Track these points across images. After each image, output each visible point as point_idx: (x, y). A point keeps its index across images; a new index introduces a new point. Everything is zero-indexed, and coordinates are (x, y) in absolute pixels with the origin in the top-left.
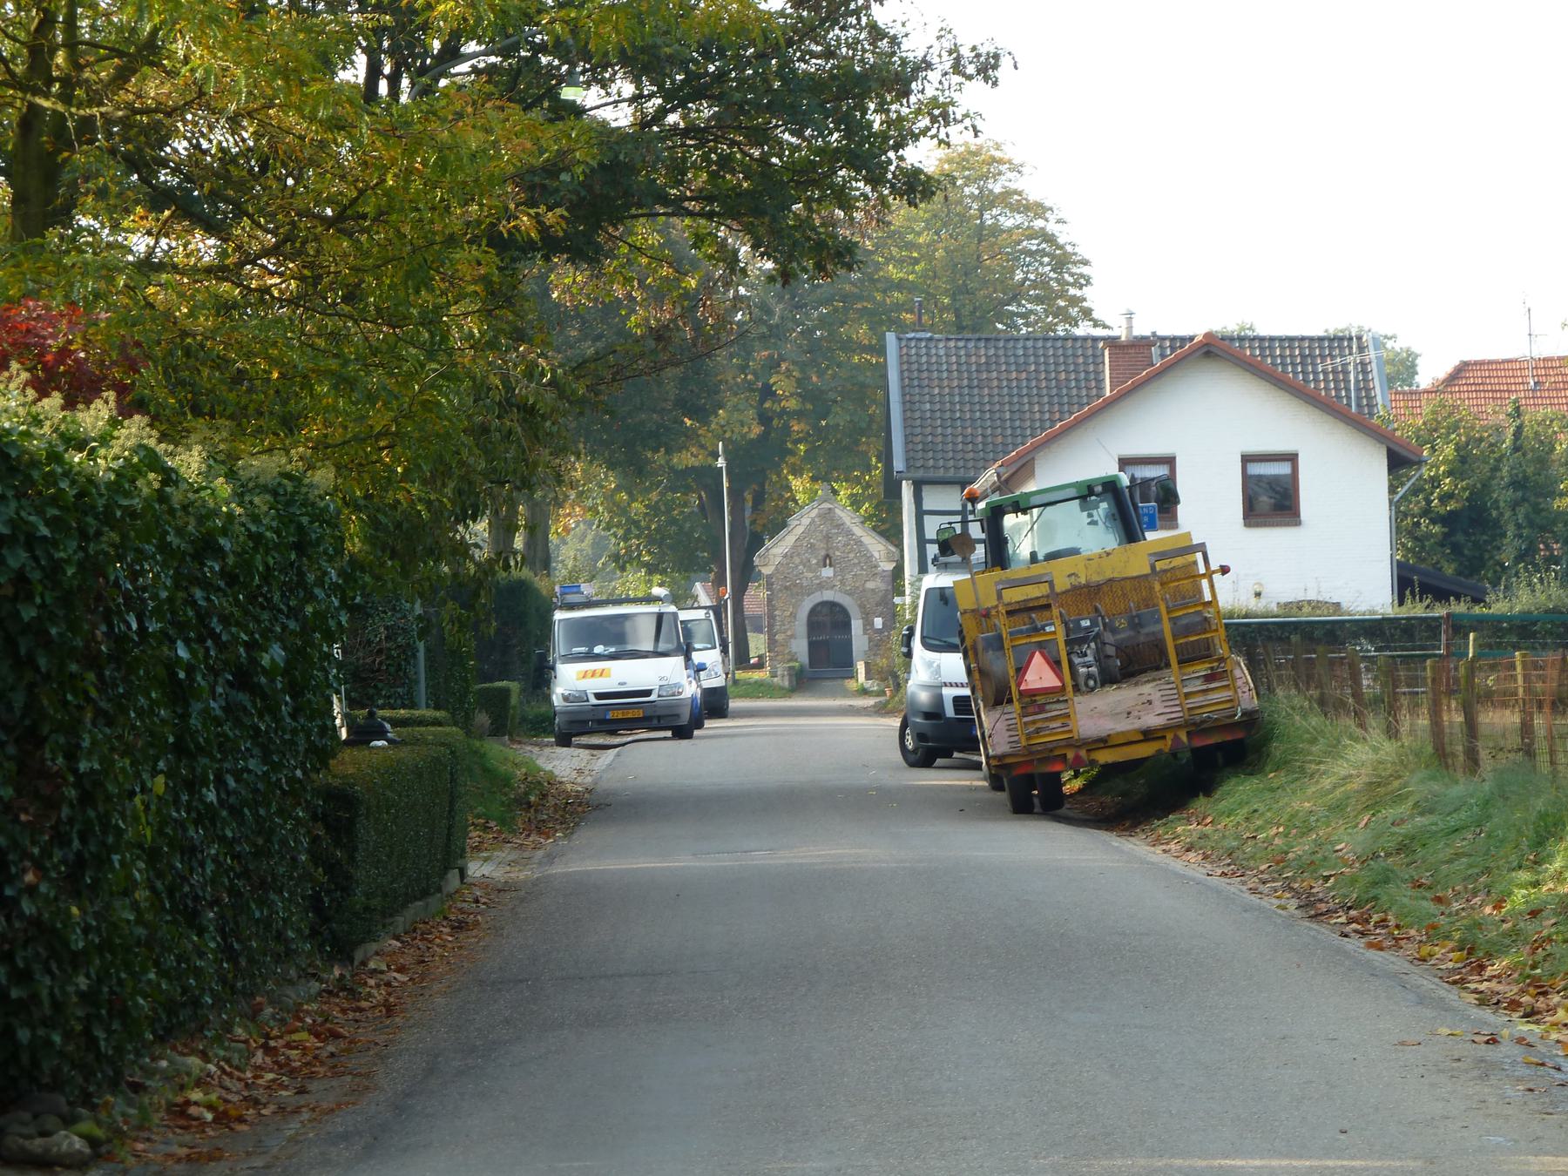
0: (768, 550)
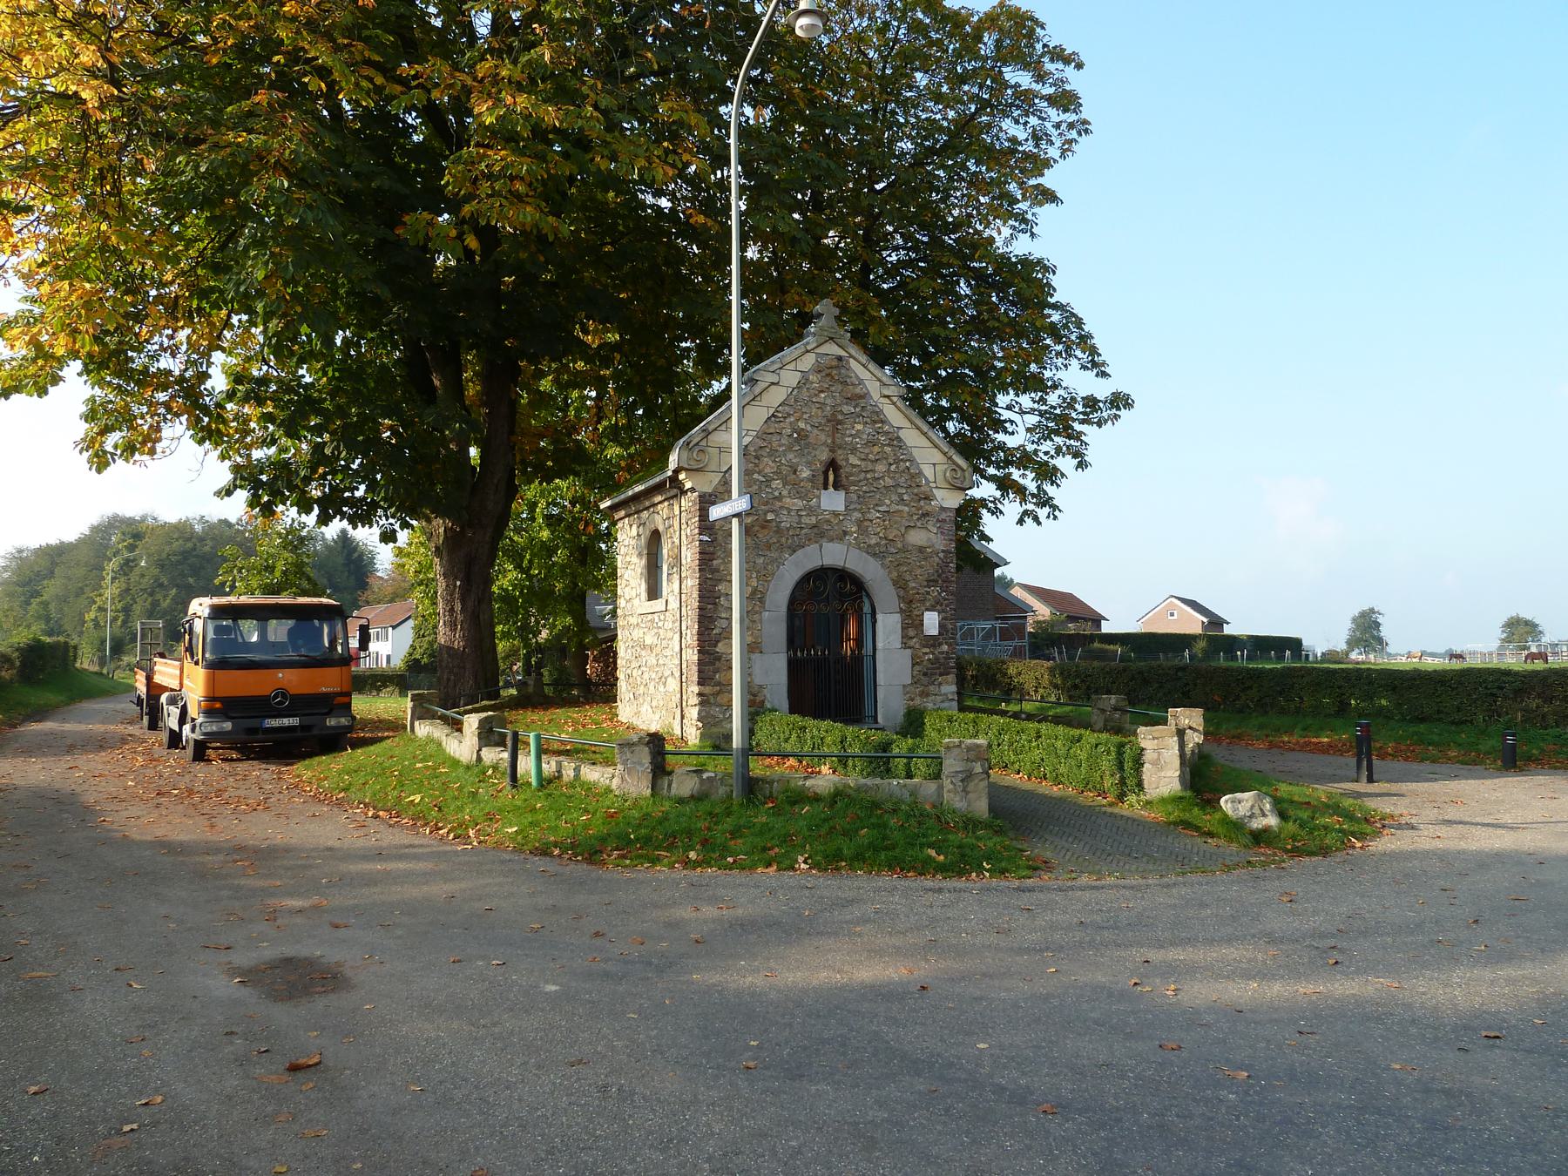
0: (707, 433)
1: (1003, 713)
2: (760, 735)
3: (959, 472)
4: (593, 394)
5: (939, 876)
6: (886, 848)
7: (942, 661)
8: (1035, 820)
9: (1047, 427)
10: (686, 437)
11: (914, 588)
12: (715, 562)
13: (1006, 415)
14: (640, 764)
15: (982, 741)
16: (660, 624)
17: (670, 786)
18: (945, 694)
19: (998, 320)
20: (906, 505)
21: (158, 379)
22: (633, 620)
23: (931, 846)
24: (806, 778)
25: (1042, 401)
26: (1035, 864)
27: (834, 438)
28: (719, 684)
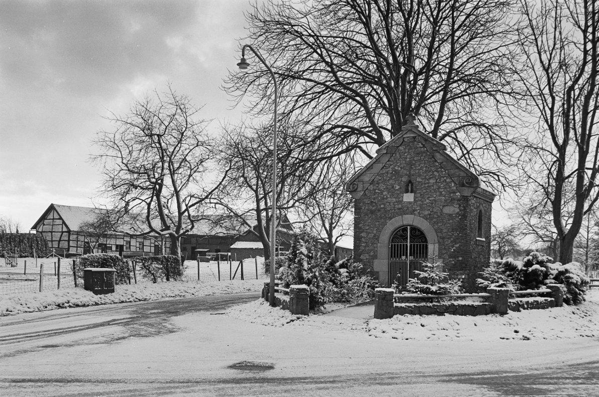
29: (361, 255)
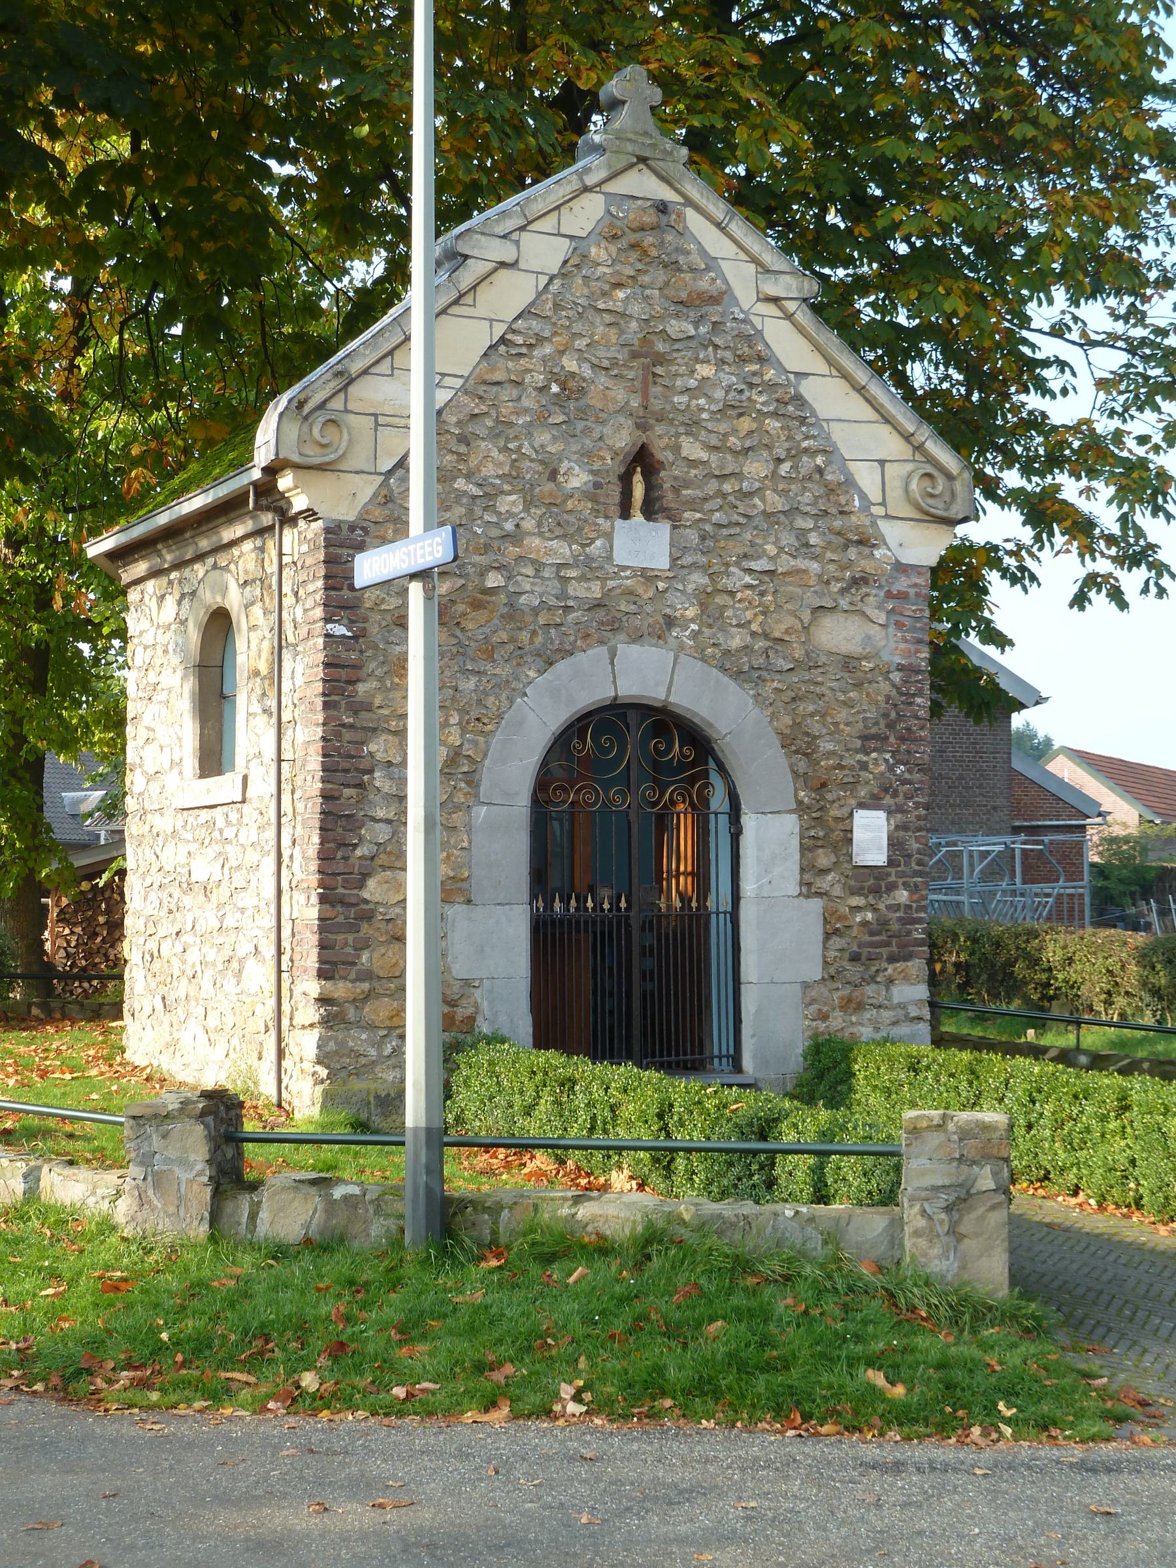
0: (346, 381)
1: (1037, 1052)
2: (463, 1098)
3: (941, 482)
4: (65, 285)
5: (894, 1435)
6: (768, 1367)
7: (895, 927)
8: (1117, 1303)
9: (1146, 378)
10: (297, 388)
11: (830, 754)
12: (361, 688)
13: (1048, 347)
14: (184, 1163)
15: (993, 1116)
16: (229, 833)
17: (253, 1216)
18: (903, 1006)
19: (1034, 122)
20: (815, 558)
21: (893, 119)
22: (164, 824)
23: (872, 1362)
24: (577, 1200)
25: (1135, 315)
26: (1120, 1408)
27: (645, 395)
28: (367, 975)
29: (365, 876)
